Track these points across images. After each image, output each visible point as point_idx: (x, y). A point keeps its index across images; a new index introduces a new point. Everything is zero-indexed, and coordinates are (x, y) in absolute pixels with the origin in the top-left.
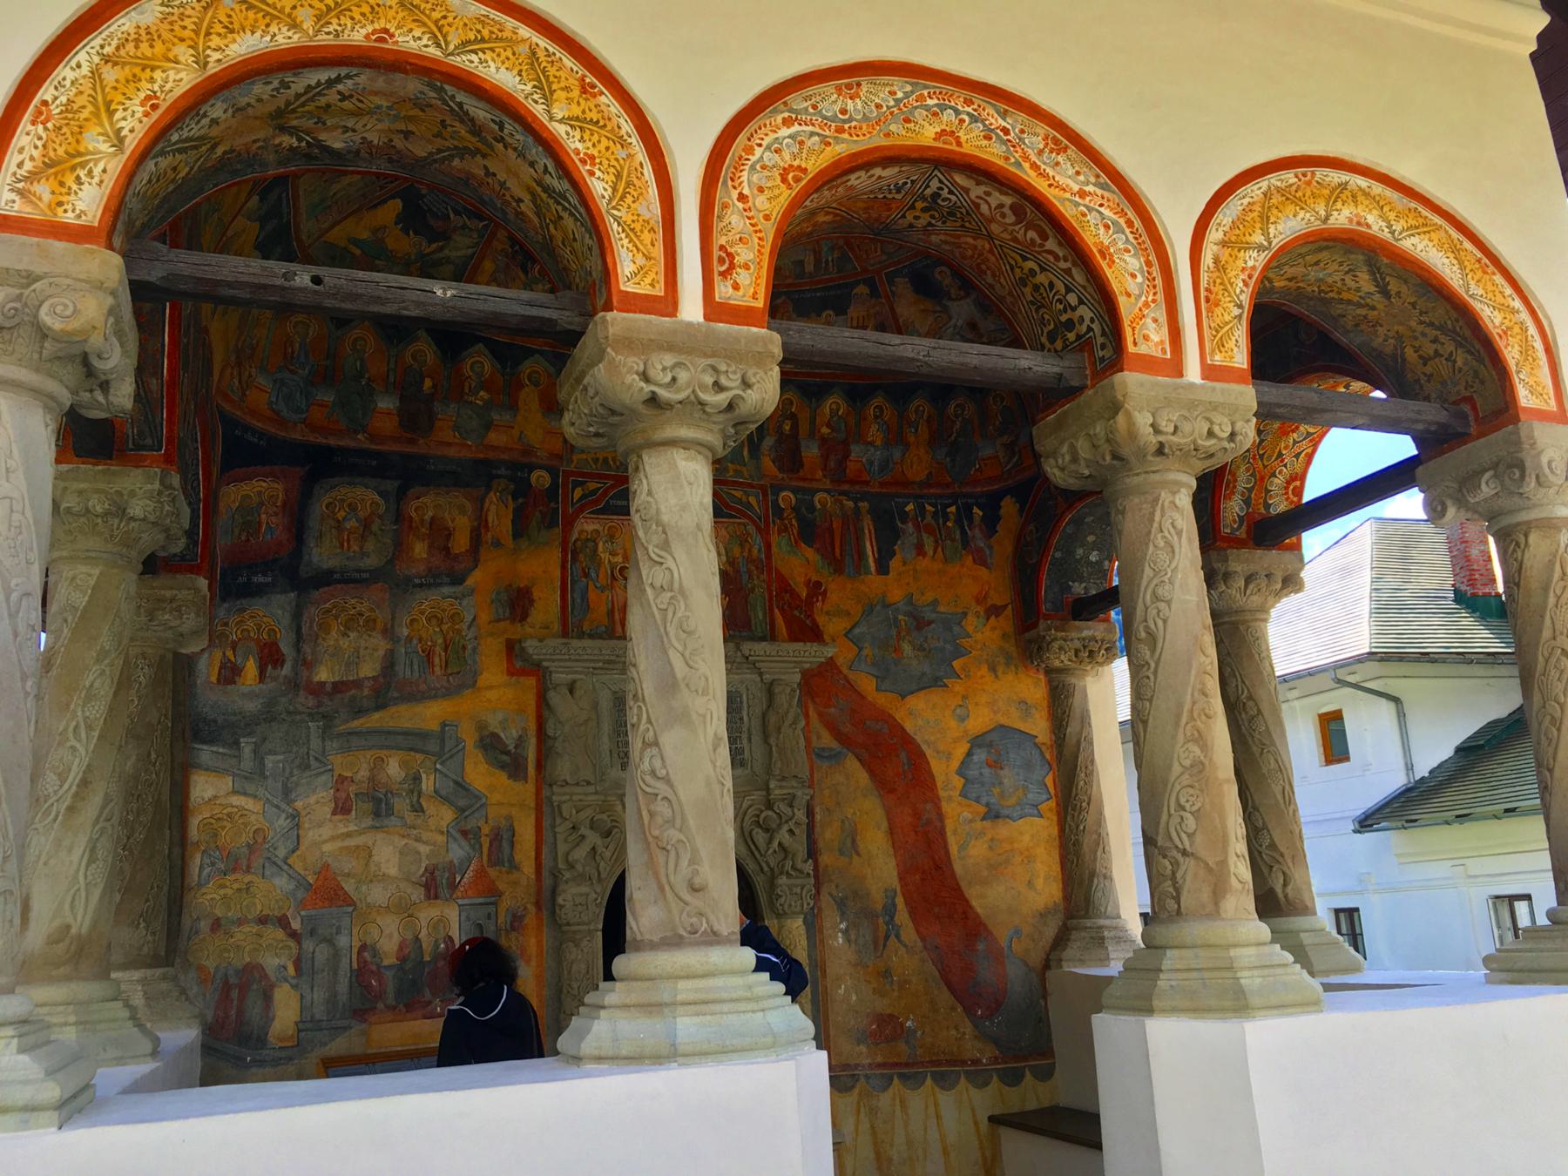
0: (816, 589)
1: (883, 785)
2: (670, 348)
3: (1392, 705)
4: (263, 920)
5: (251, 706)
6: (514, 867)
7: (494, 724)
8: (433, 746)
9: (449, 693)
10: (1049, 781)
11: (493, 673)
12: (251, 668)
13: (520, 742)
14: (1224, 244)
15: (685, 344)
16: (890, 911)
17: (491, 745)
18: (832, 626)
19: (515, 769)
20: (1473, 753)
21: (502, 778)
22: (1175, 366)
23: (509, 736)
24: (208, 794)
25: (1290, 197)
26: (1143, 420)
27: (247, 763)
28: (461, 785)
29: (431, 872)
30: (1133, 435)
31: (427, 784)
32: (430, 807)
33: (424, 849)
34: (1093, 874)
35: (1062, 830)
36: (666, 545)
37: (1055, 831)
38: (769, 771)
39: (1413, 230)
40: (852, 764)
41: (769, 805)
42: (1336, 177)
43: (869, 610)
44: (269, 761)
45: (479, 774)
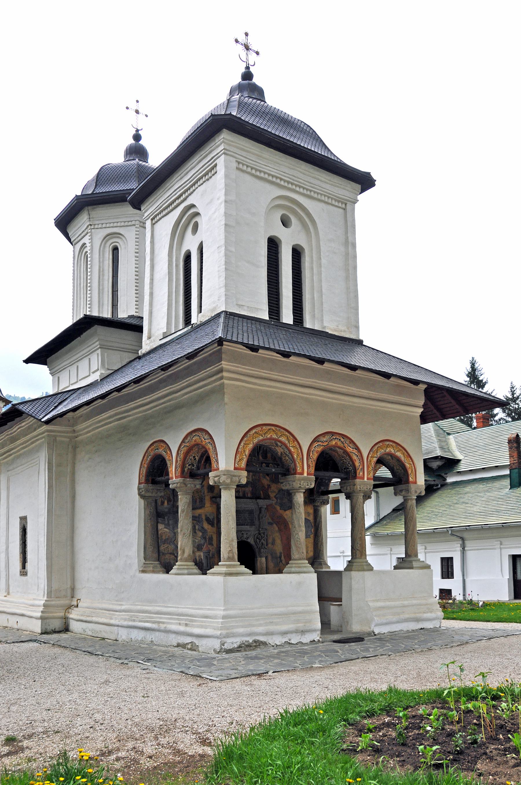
0: (269, 486)
1: (280, 530)
2: (303, 480)
3: (225, 137)
4: (171, 554)
5: (166, 510)
6: (212, 545)
7: (208, 516)
8: (197, 519)
9: (200, 508)
10: (312, 530)
11: (208, 504)
12: (166, 502)
13: (213, 519)
14: (371, 457)
15: (304, 479)
16: (280, 557)
17: (208, 520)
18: (272, 495)
19: (212, 525)
20: (395, 510)
21: (210, 526)
22: (363, 478)
23: (211, 518)
24: (161, 528)
25: (380, 447)
26: (358, 487)
27: (166, 522)
28: (203, 528)
29: (198, 545)
30: (357, 489)
31: (197, 527)
32: (197, 532)
33: (197, 541)
34: (320, 550)
35: (314, 541)
36: (299, 507)
37: (313, 541)
38: (259, 527)
39: (398, 451)
40: (275, 525)
41: (260, 534)
42: (388, 443)
43: (279, 491)
44: (170, 521)
45: (206, 526)
